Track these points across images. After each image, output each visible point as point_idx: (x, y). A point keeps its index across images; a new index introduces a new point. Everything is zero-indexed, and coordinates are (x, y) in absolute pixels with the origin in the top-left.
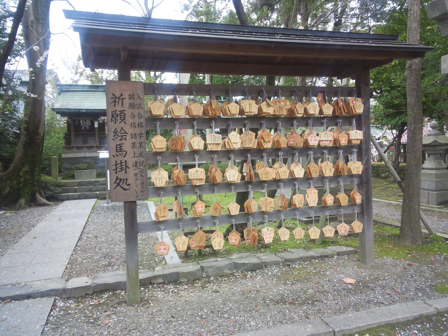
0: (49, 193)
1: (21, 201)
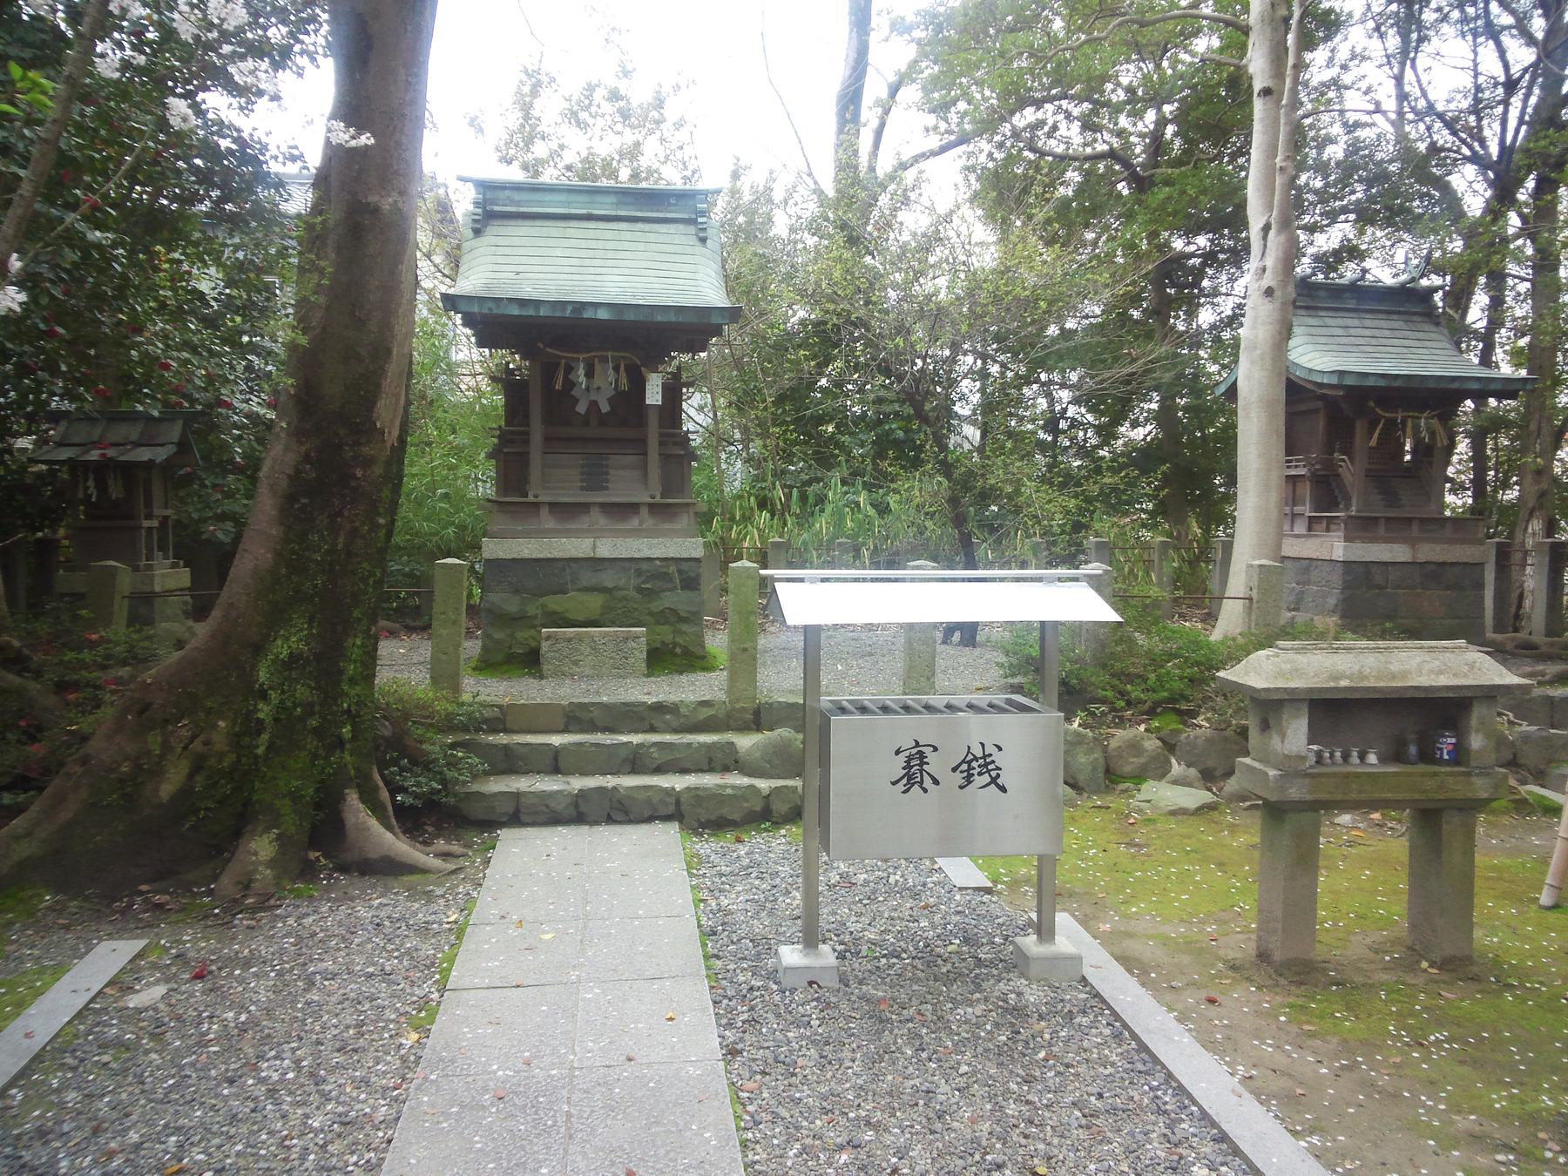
0: (420, 784)
1: (253, 845)
